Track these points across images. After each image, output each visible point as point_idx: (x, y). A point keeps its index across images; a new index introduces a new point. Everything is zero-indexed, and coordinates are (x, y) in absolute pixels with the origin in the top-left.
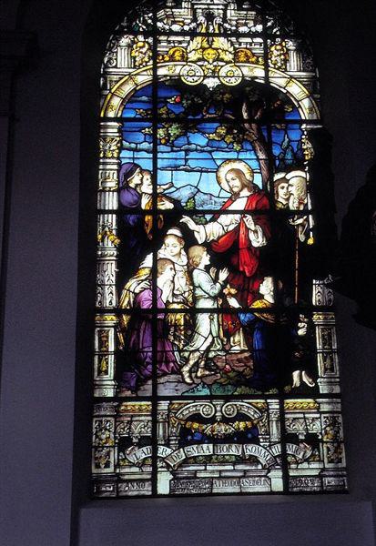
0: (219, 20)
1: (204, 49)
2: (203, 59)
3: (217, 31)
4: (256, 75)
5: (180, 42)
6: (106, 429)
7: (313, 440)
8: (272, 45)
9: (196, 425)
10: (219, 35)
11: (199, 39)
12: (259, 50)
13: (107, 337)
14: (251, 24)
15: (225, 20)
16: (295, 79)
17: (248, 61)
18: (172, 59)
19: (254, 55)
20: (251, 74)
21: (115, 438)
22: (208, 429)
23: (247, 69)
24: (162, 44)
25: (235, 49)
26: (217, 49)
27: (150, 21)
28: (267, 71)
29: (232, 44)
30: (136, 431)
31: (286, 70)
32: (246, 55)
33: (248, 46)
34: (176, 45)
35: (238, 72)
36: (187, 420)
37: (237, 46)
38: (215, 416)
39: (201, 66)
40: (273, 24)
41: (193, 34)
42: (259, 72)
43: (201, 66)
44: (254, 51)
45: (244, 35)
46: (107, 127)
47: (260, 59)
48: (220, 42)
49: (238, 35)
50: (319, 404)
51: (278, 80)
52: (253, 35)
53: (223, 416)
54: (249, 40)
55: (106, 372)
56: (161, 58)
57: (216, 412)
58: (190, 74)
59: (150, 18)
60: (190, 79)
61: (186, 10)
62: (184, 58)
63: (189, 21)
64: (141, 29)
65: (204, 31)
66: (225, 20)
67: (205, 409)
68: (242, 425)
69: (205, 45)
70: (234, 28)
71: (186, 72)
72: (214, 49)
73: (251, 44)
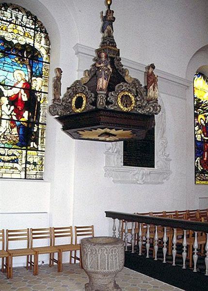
10: (20, 25)
41: (10, 22)
48: (19, 28)
51: (37, 46)
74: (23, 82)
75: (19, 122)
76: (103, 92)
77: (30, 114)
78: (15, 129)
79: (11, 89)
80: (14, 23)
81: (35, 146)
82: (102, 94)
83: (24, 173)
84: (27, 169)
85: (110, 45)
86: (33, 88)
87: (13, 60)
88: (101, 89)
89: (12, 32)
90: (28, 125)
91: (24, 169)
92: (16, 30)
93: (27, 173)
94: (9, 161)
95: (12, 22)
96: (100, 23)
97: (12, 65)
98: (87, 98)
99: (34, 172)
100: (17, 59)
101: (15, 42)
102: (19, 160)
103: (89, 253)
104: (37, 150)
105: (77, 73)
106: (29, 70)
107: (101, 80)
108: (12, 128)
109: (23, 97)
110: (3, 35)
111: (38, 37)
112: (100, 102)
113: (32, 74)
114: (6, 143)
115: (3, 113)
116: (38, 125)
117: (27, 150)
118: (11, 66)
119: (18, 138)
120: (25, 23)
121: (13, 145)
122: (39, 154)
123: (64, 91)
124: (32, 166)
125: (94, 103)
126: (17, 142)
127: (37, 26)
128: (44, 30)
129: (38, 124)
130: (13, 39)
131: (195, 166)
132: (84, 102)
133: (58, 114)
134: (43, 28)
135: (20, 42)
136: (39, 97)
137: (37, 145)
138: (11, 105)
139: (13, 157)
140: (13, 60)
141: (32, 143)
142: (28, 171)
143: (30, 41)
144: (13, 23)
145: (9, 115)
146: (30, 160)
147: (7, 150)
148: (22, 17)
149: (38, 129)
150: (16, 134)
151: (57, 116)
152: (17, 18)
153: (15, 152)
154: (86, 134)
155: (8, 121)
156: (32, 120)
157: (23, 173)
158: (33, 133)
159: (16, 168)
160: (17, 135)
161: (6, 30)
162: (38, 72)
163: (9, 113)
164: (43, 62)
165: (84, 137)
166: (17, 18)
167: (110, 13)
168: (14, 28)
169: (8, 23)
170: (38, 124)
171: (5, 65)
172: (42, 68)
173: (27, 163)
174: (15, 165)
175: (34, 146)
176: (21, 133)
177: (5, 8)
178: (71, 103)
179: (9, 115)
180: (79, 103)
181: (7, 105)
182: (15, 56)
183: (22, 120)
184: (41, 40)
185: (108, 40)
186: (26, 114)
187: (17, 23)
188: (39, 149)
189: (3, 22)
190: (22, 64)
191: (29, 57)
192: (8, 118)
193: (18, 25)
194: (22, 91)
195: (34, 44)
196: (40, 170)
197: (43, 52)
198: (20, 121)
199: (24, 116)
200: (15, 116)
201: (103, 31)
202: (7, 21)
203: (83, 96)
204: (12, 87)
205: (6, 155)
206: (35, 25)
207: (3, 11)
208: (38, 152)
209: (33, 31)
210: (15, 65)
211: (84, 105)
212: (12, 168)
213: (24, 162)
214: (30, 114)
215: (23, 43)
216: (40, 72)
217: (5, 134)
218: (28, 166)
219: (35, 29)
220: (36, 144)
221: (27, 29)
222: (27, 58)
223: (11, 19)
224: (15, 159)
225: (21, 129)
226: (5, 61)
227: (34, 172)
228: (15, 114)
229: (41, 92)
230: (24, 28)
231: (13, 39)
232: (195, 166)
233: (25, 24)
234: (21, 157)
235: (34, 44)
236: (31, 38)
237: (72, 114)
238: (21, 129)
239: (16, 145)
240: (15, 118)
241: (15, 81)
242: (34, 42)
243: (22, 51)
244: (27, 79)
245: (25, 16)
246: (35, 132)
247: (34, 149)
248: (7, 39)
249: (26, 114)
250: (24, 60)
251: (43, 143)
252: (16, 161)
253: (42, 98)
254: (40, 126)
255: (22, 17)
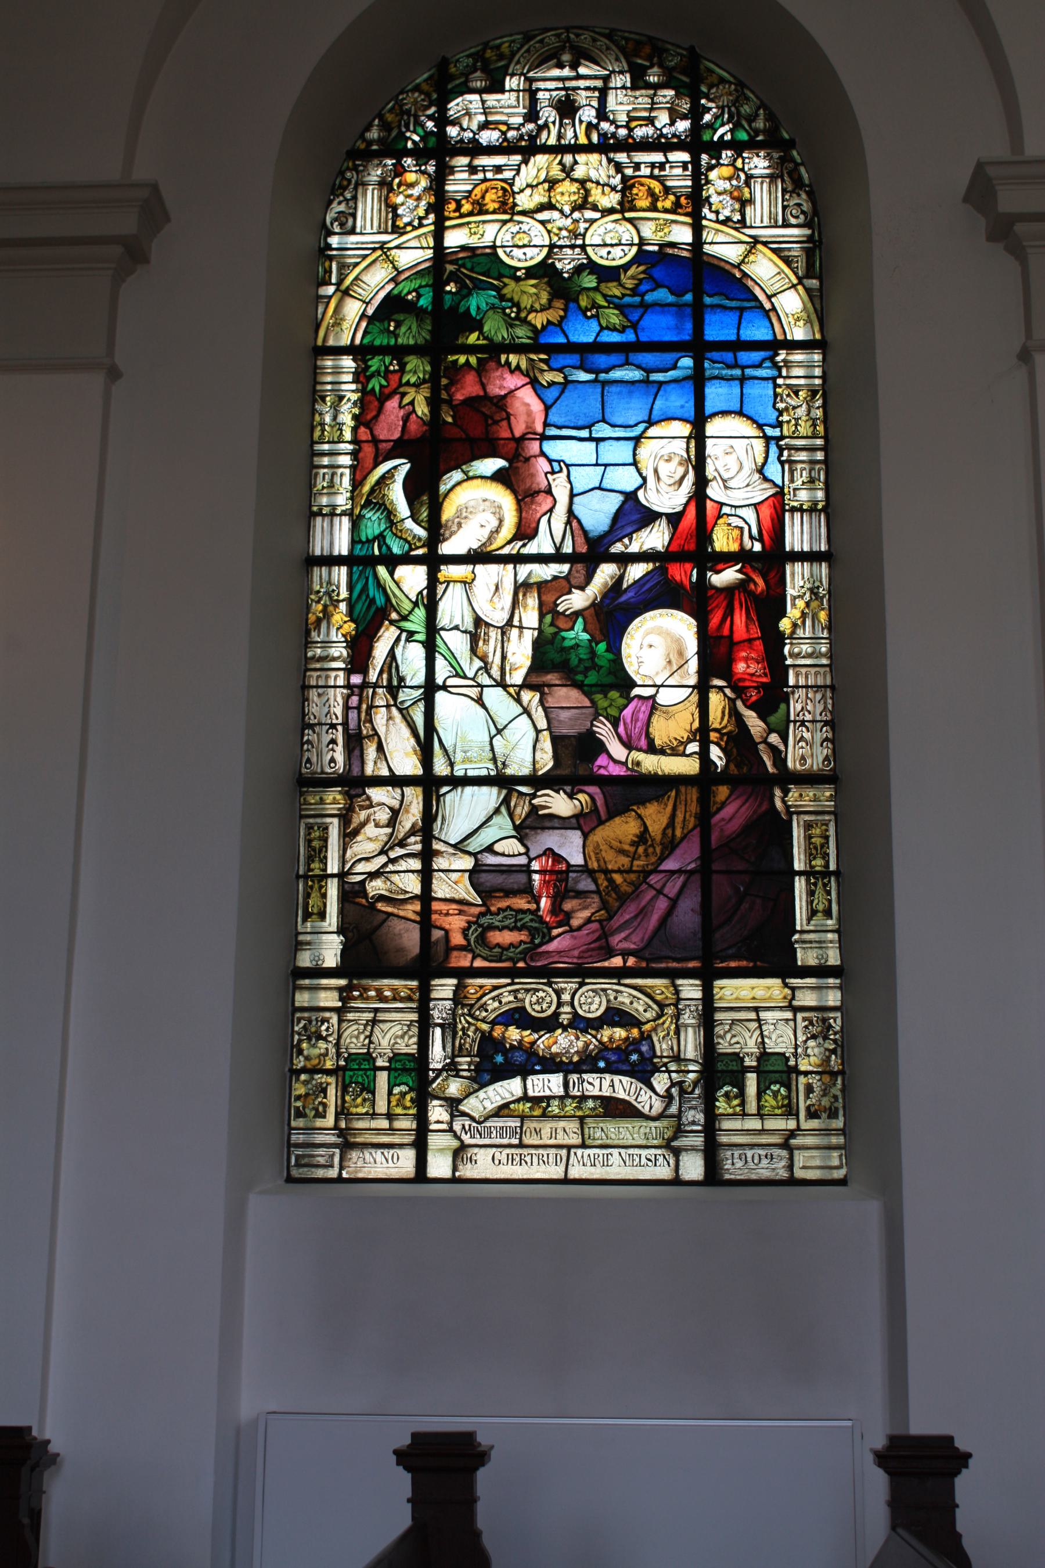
0: (588, 114)
1: (552, 183)
2: (549, 206)
3: (583, 140)
4: (672, 238)
5: (498, 169)
6: (320, 1037)
7: (776, 1070)
8: (711, 168)
9: (514, 1034)
10: (589, 148)
11: (541, 160)
12: (680, 181)
13: (325, 840)
14: (663, 118)
15: (602, 114)
16: (765, 244)
17: (653, 208)
18: (480, 209)
19: (667, 190)
20: (659, 237)
21: (338, 1054)
22: (544, 1042)
23: (651, 225)
24: (458, 176)
25: (625, 179)
26: (582, 182)
27: (430, 124)
28: (697, 229)
29: (619, 167)
30: (385, 1043)
31: (743, 221)
32: (651, 193)
33: (656, 172)
34: (489, 175)
35: (627, 232)
36: (493, 1023)
37: (629, 172)
38: (556, 1014)
39: (543, 223)
40: (716, 117)
41: (529, 148)
42: (683, 235)
43: (543, 223)
44: (669, 184)
45: (645, 145)
46: (769, 167)
47: (683, 200)
48: (591, 166)
49: (630, 146)
50: (793, 989)
51: (724, 247)
52: (661, 144)
53: (575, 1014)
54: (658, 157)
55: (322, 915)
56: (452, 206)
57: (560, 1004)
58: (523, 243)
59: (430, 118)
60: (517, 253)
61: (514, 95)
62: (508, 207)
63: (520, 120)
64: (410, 145)
65: (552, 141)
66: (602, 114)
67: (539, 999)
68: (620, 1033)
69: (556, 172)
70: (623, 132)
71: (508, 236)
72: (576, 180)
73: (662, 166)
110: (488, 240)
122: (807, 999)
131: (489, 42)
146: (740, 1041)
205: (564, 1019)
232: (489, 42)
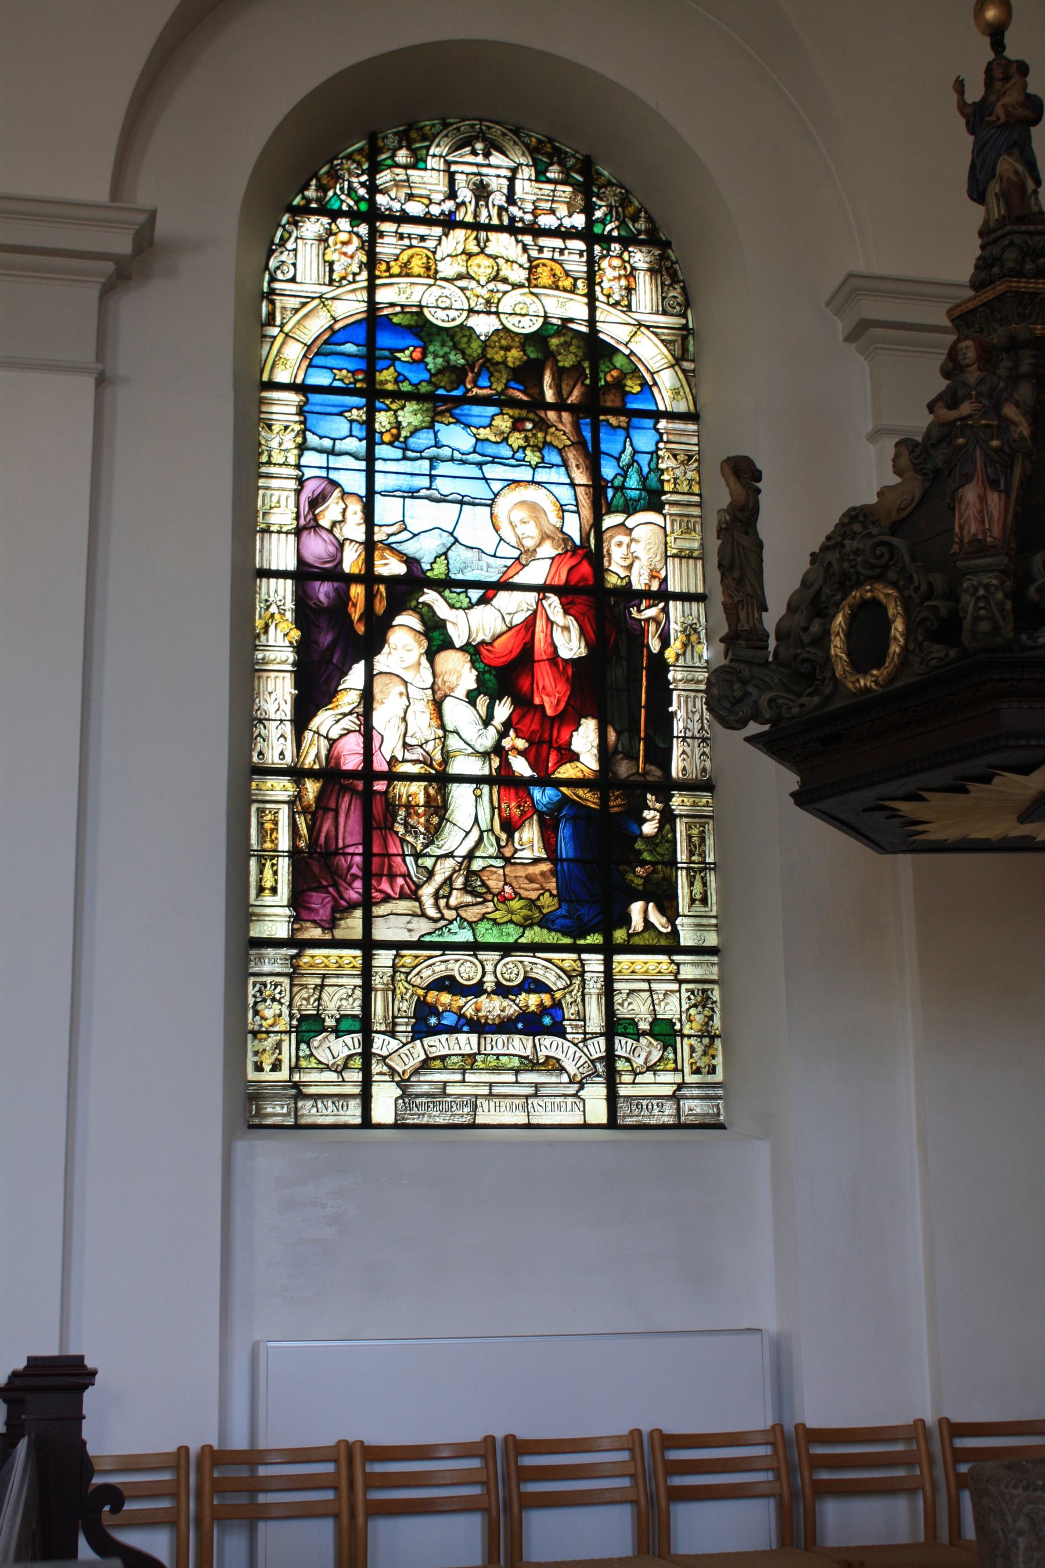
10: (500, 229)
41: (448, 223)
48: (501, 244)
51: (613, 328)
74: (548, 550)
75: (550, 792)
76: (988, 560)
77: (612, 736)
78: (530, 835)
79: (484, 600)
80: (469, 218)
81: (656, 918)
82: (985, 570)
83: (602, 1091)
84: (620, 1065)
85: (1029, 266)
86: (612, 580)
87: (484, 433)
88: (979, 547)
89: (460, 277)
90: (604, 800)
91: (600, 1068)
92: (481, 259)
93: (623, 1091)
94: (506, 1026)
95: (459, 217)
96: (961, 145)
97: (480, 465)
98: (906, 603)
99: (664, 1083)
100: (504, 423)
101: (483, 325)
102: (570, 1012)
103: (1022, 1542)
104: (671, 947)
105: (871, 449)
106: (581, 477)
107: (970, 494)
108: (510, 827)
109: (558, 637)
110: (414, 300)
111: (610, 273)
112: (977, 619)
113: (601, 498)
114: (483, 917)
115: (453, 742)
116: (666, 799)
117: (609, 950)
118: (474, 471)
119: (552, 885)
120: (529, 207)
121: (526, 925)
122: (686, 973)
123: (782, 576)
124: (649, 1050)
125: (947, 630)
126: (548, 903)
127: (598, 214)
128: (642, 225)
129: (665, 788)
130: (471, 311)
132: (837, 646)
133: (757, 717)
134: (635, 219)
135: (511, 323)
136: (652, 627)
137: (670, 912)
138: (495, 697)
139: (532, 1001)
140: (484, 433)
141: (636, 909)
142: (627, 1078)
143: (576, 309)
144: (463, 225)
145: (485, 755)
146: (636, 1008)
147: (490, 957)
148: (512, 180)
149: (668, 817)
150: (536, 861)
151: (754, 728)
152: (482, 192)
153: (540, 968)
154: (941, 815)
155: (486, 789)
156: (623, 769)
157: (596, 1096)
158: (639, 845)
159: (553, 1065)
160: (545, 867)
161: (431, 272)
162: (633, 481)
163: (487, 739)
164: (657, 415)
165: (935, 833)
166: (482, 192)
167: (1007, 78)
168: (473, 247)
169: (438, 231)
170: (665, 788)
171: (442, 468)
172: (654, 454)
173: (615, 1026)
174: (549, 1046)
175: (648, 925)
176: (565, 849)
177: (414, 152)
178: (823, 640)
179: (485, 755)
180: (869, 627)
181: (471, 698)
182: (492, 410)
183: (567, 771)
184: (629, 290)
185: (1011, 244)
186: (585, 739)
187: (483, 219)
188: (687, 938)
189: (406, 229)
190: (539, 449)
191: (574, 398)
192: (486, 771)
193: (489, 228)
194: (553, 604)
195: (592, 321)
196: (697, 1071)
197: (651, 353)
198: (558, 783)
199: (575, 747)
200: (521, 753)
201: (977, 194)
202: (427, 220)
203: (886, 594)
204: (490, 590)
205: (489, 986)
206: (588, 210)
207: (406, 167)
208: (677, 958)
209: (580, 245)
210: (495, 460)
211: (895, 649)
212: (531, 1064)
213: (596, 1021)
214: (612, 736)
215: (529, 326)
216: (644, 479)
217: (477, 865)
218: (623, 1046)
219: (587, 235)
220: (661, 910)
221: (543, 241)
222: (559, 406)
223: (449, 205)
224: (543, 1010)
225: (565, 832)
226: (437, 445)
227: (664, 1083)
228: (521, 744)
229: (663, 595)
230: (528, 239)
231: (471, 311)
233: (529, 217)
234: (576, 993)
235: (592, 321)
236: (573, 290)
237: (836, 705)
238: (565, 832)
239: (546, 922)
240: (521, 767)
241: (505, 550)
242: (592, 308)
243: (527, 375)
244: (573, 527)
245: (527, 172)
246: (648, 839)
247: (648, 939)
248: (438, 318)
249: (585, 739)
250: (543, 425)
251: (704, 901)
252: (547, 1021)
253: (674, 627)
254: (679, 802)
255: (512, 180)
